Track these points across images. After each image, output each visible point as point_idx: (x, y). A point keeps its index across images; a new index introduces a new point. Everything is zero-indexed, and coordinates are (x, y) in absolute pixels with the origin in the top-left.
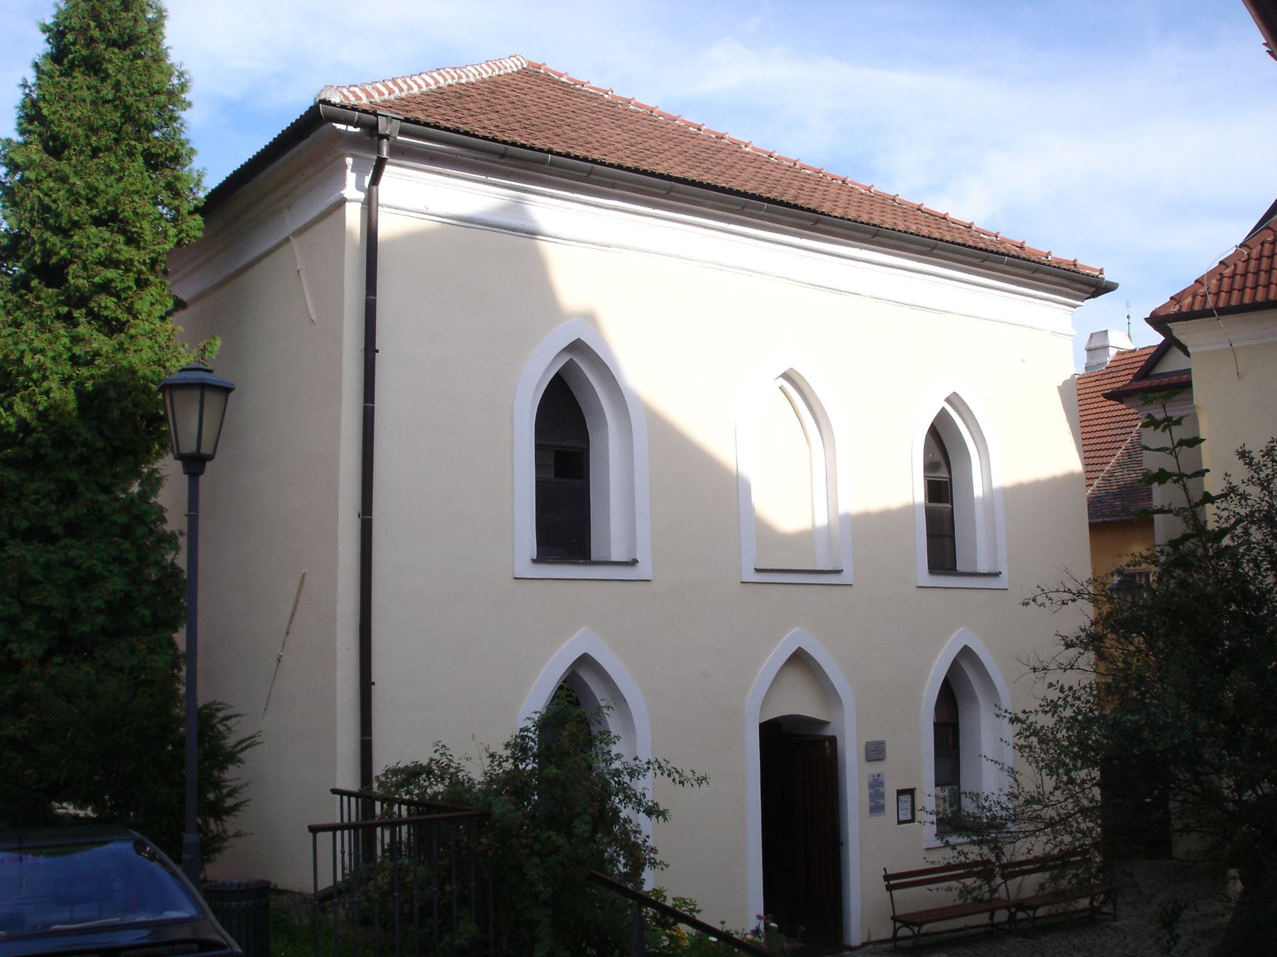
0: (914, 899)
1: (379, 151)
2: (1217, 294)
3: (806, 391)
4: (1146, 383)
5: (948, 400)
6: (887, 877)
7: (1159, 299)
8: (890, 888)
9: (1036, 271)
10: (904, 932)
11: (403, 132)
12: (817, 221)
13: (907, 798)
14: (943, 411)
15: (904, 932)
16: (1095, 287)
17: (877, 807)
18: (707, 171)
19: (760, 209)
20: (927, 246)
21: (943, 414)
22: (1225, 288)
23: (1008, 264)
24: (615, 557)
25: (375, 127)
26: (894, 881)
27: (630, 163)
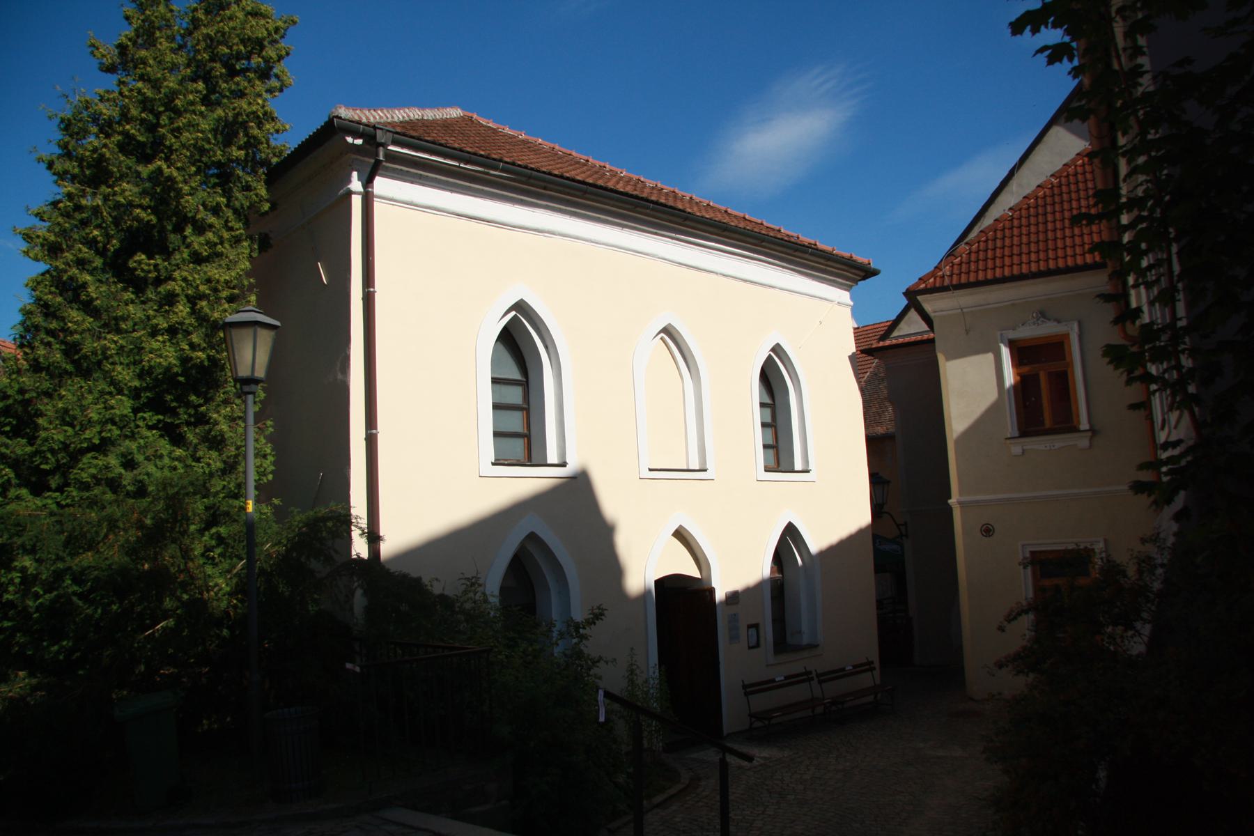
0: (761, 702)
1: (377, 155)
2: (951, 276)
3: (676, 336)
4: (888, 343)
5: (773, 350)
6: (745, 687)
7: (911, 281)
8: (746, 694)
9: (796, 250)
10: (758, 724)
11: (395, 143)
12: (585, 192)
13: (753, 631)
14: (770, 356)
15: (758, 724)
16: (867, 273)
17: (734, 637)
18: (590, 176)
19: (648, 208)
20: (631, 204)
21: (769, 358)
22: (956, 271)
23: (653, 209)
24: (797, 468)
25: (374, 137)
26: (750, 689)
27: (556, 172)
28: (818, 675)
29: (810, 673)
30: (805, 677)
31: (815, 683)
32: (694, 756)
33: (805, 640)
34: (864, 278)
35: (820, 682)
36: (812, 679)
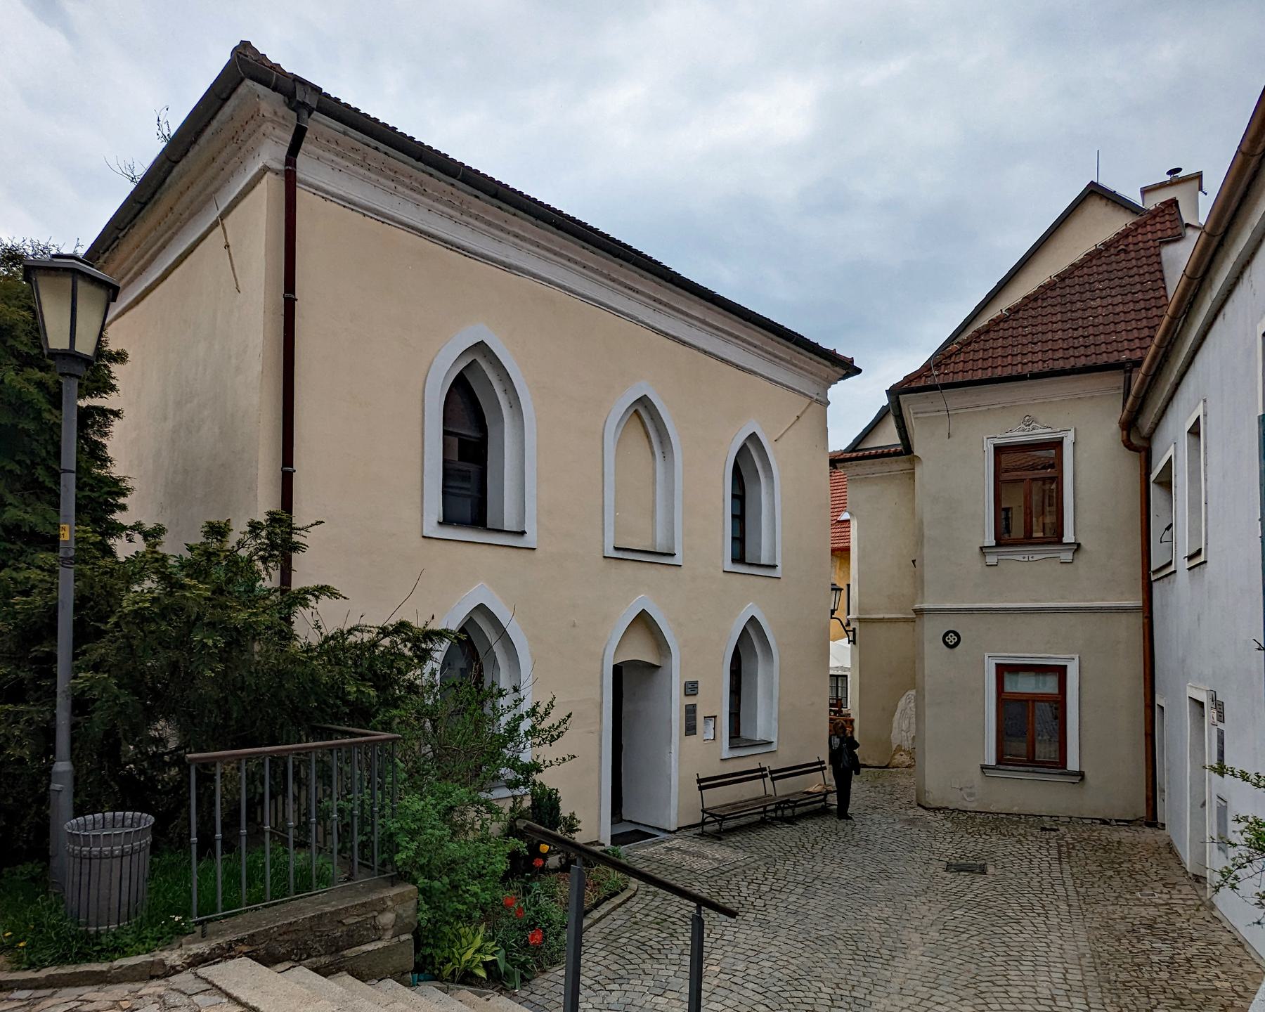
6: (699, 781)
8: (701, 788)
28: (771, 772)
29: (765, 769)
30: (760, 773)
31: (768, 780)
32: (642, 852)
33: (760, 735)
34: (845, 377)
35: (773, 779)
36: (766, 776)
